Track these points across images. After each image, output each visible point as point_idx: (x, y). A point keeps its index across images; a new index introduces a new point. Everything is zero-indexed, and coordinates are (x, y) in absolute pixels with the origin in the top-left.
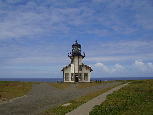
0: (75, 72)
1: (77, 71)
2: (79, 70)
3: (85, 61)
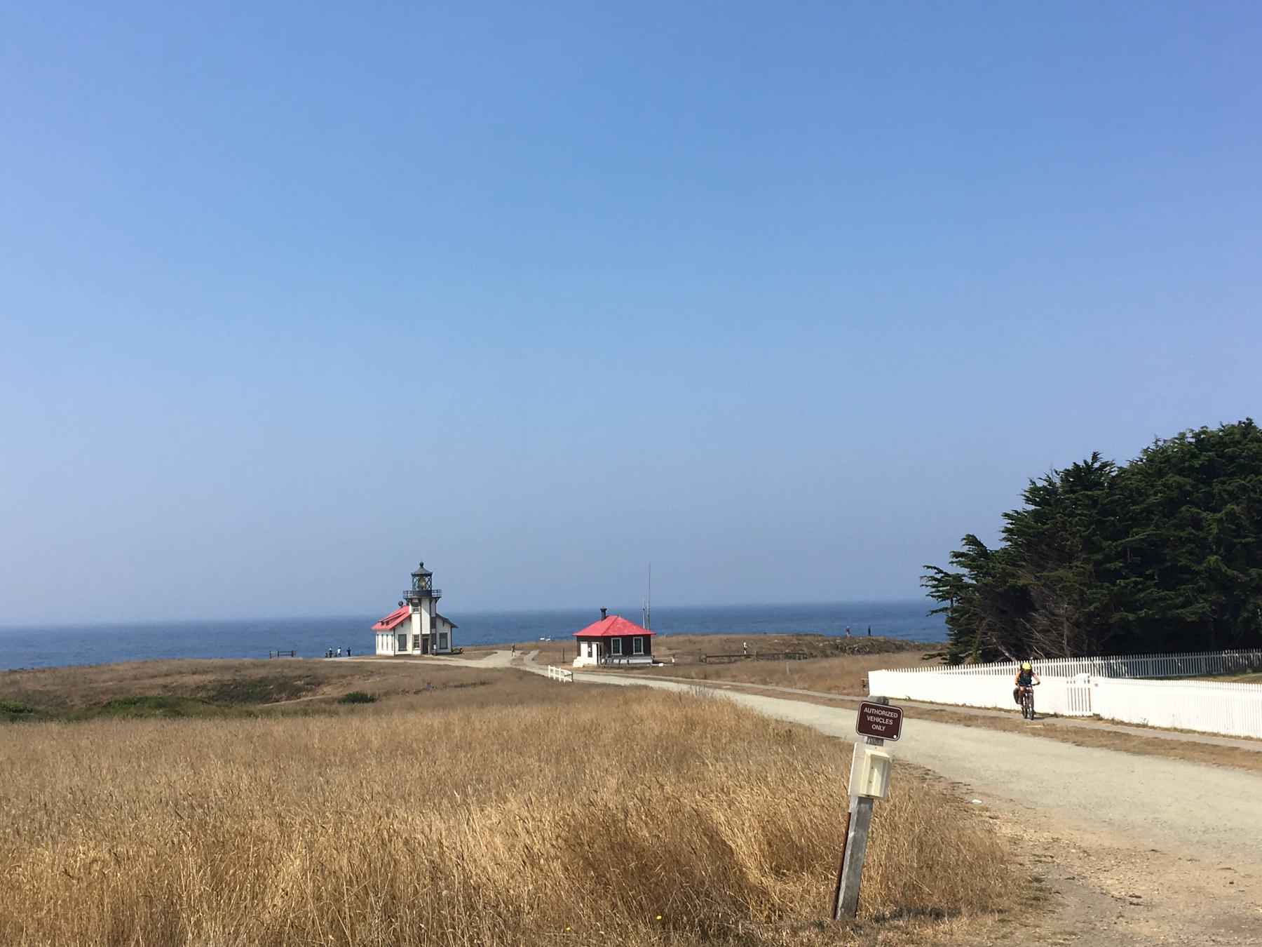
1: (427, 631)
3: (442, 608)
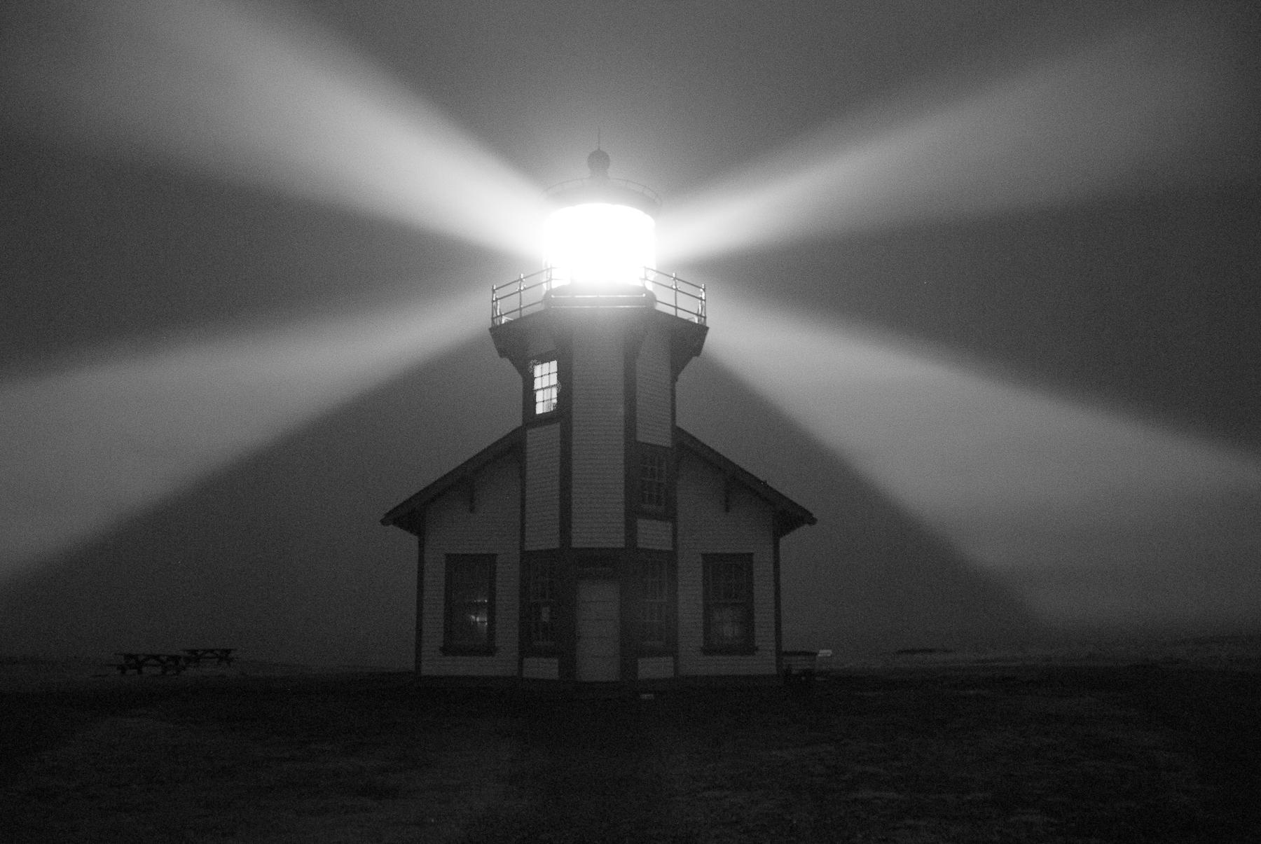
0: (577, 543)
2: (632, 514)
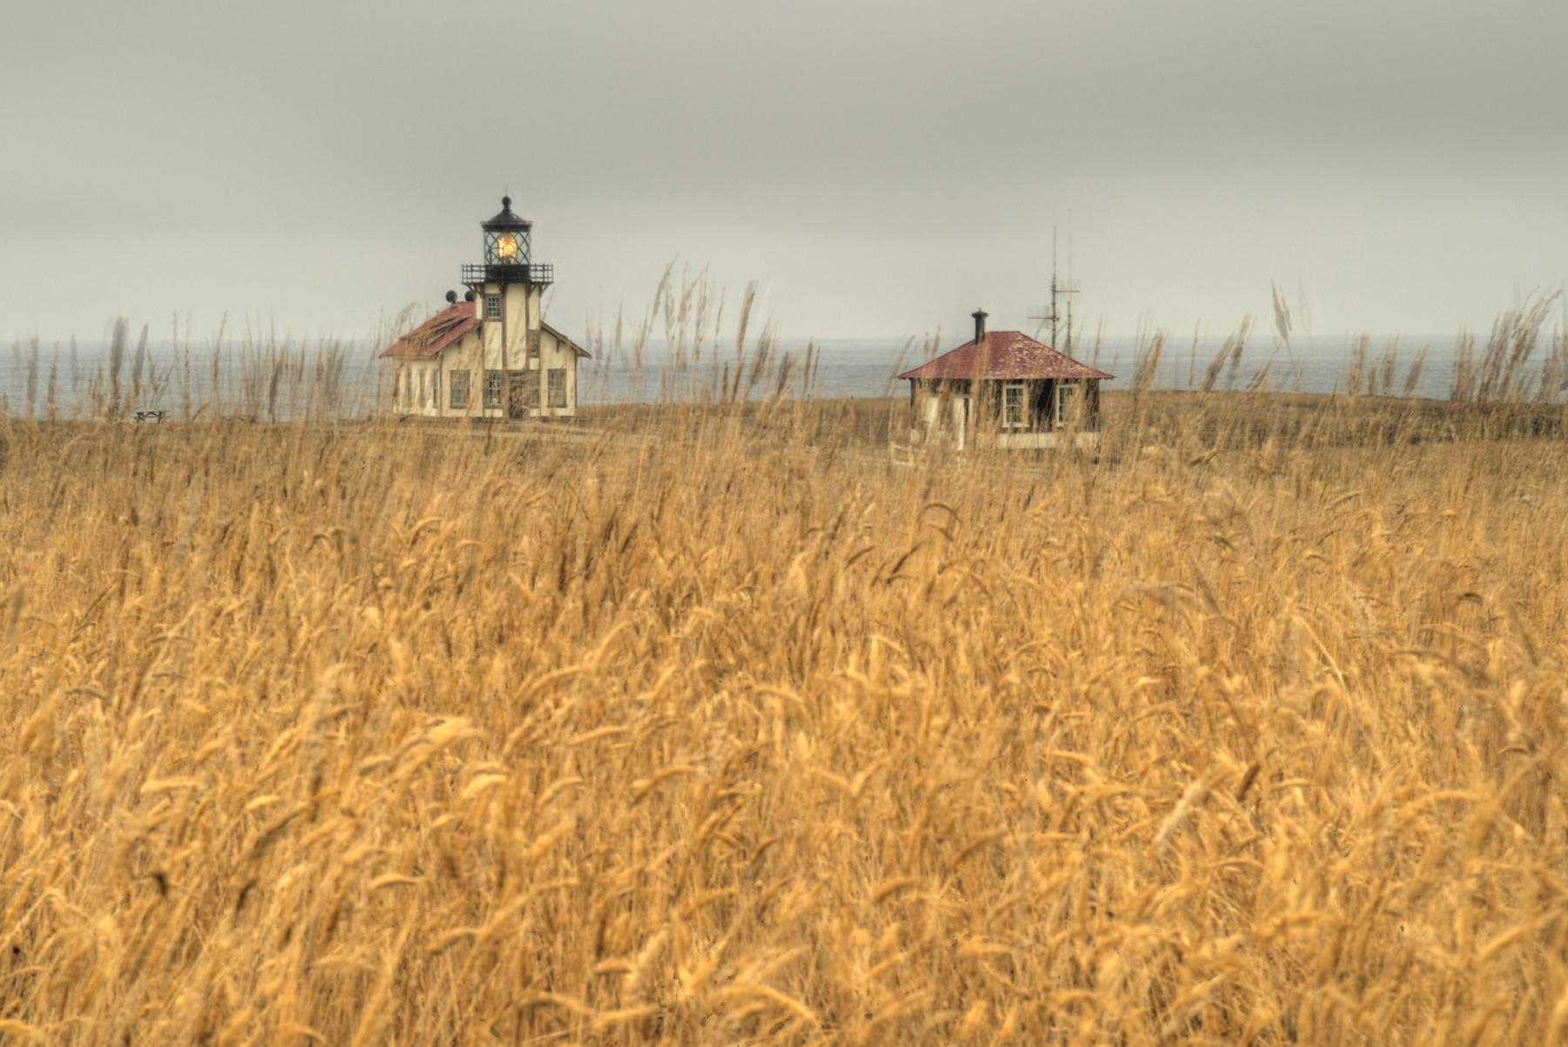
1: (518, 364)
2: (528, 357)
